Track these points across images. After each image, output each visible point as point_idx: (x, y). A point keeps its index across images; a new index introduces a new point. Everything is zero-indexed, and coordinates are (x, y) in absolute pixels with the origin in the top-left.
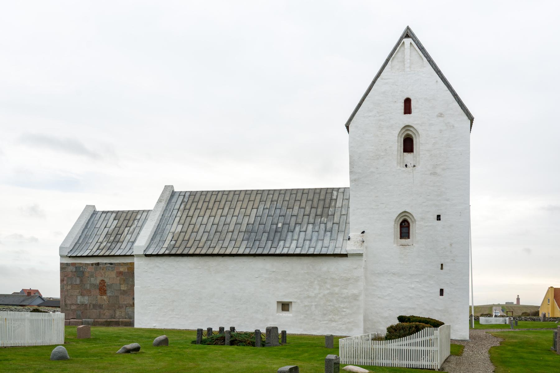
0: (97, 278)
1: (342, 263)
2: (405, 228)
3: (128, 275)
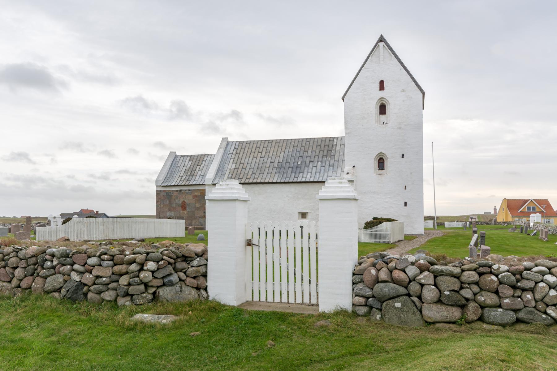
2: (381, 163)
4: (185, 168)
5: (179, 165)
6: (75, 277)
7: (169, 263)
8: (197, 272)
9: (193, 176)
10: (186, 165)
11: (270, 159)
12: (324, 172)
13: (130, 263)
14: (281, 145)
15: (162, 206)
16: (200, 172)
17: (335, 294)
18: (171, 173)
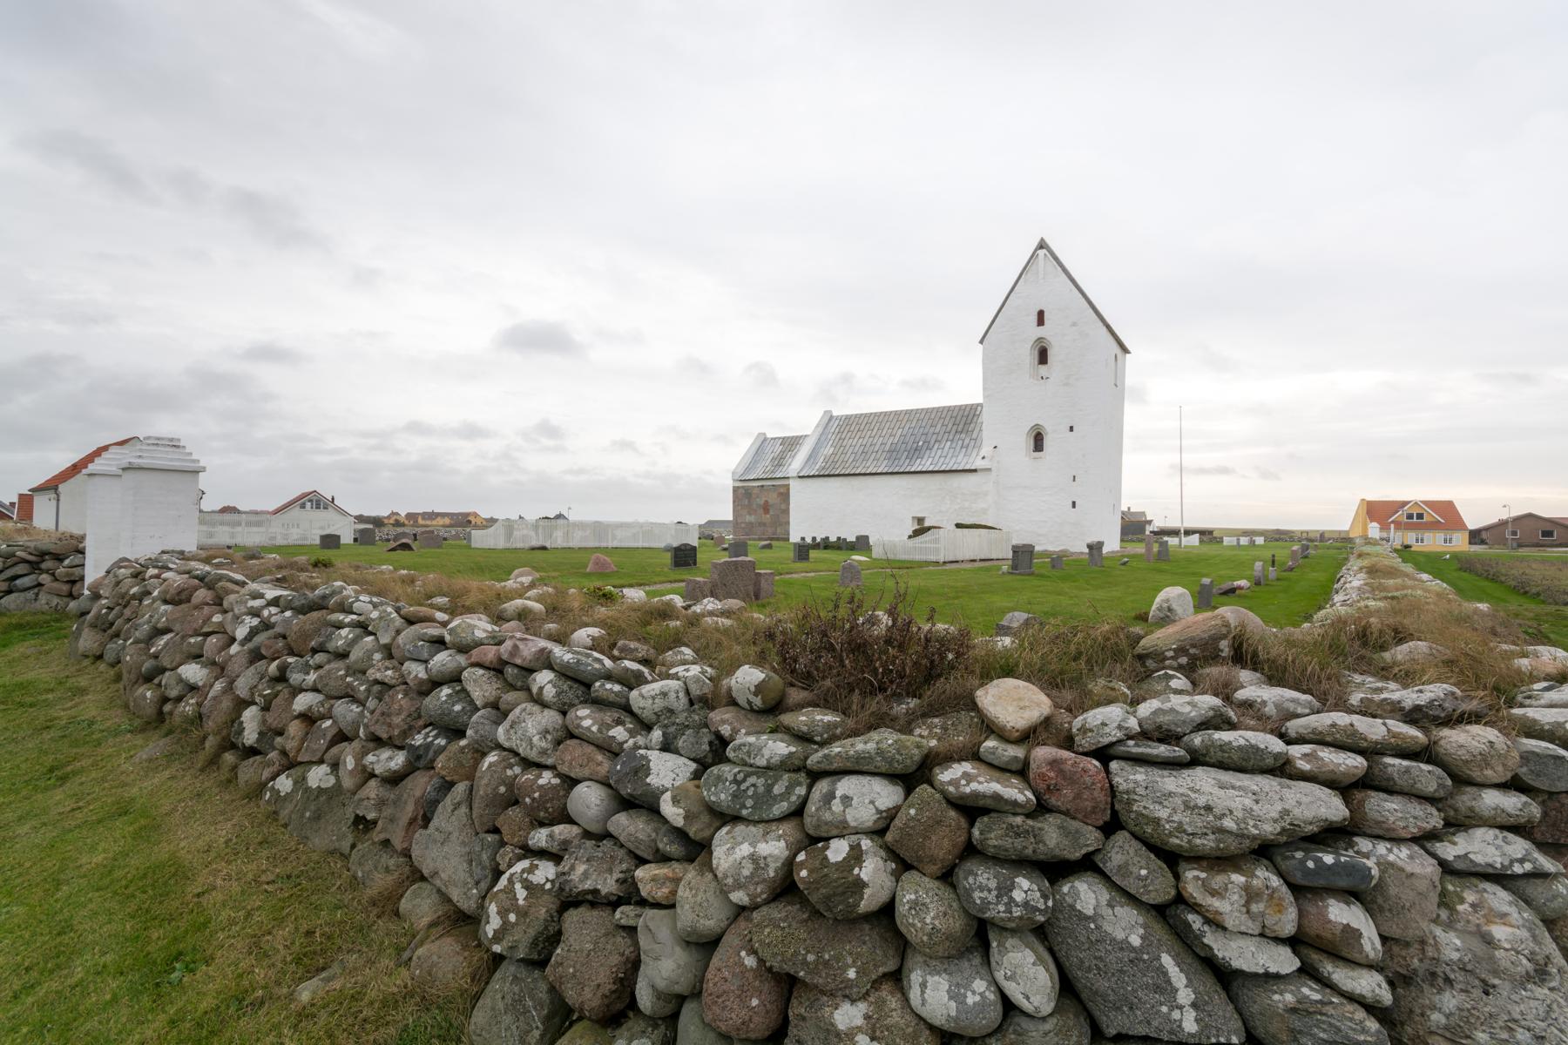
0: (761, 498)
1: (972, 477)
2: (1038, 442)
3: (785, 495)
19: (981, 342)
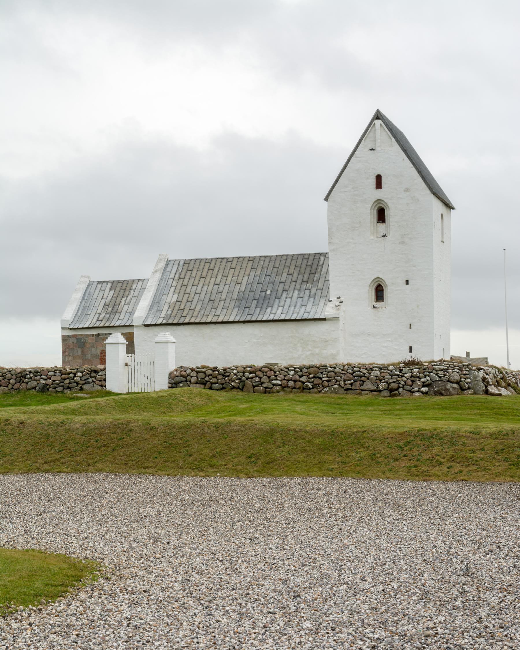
1: (322, 327)
2: (379, 292)
4: (103, 301)
5: (95, 297)
6: (43, 381)
7: (88, 374)
8: (101, 378)
9: (116, 313)
10: (105, 296)
11: (227, 286)
12: (301, 306)
13: (69, 374)
14: (244, 265)
15: (71, 358)
16: (126, 307)
17: (162, 384)
18: (84, 309)
19: (326, 199)
